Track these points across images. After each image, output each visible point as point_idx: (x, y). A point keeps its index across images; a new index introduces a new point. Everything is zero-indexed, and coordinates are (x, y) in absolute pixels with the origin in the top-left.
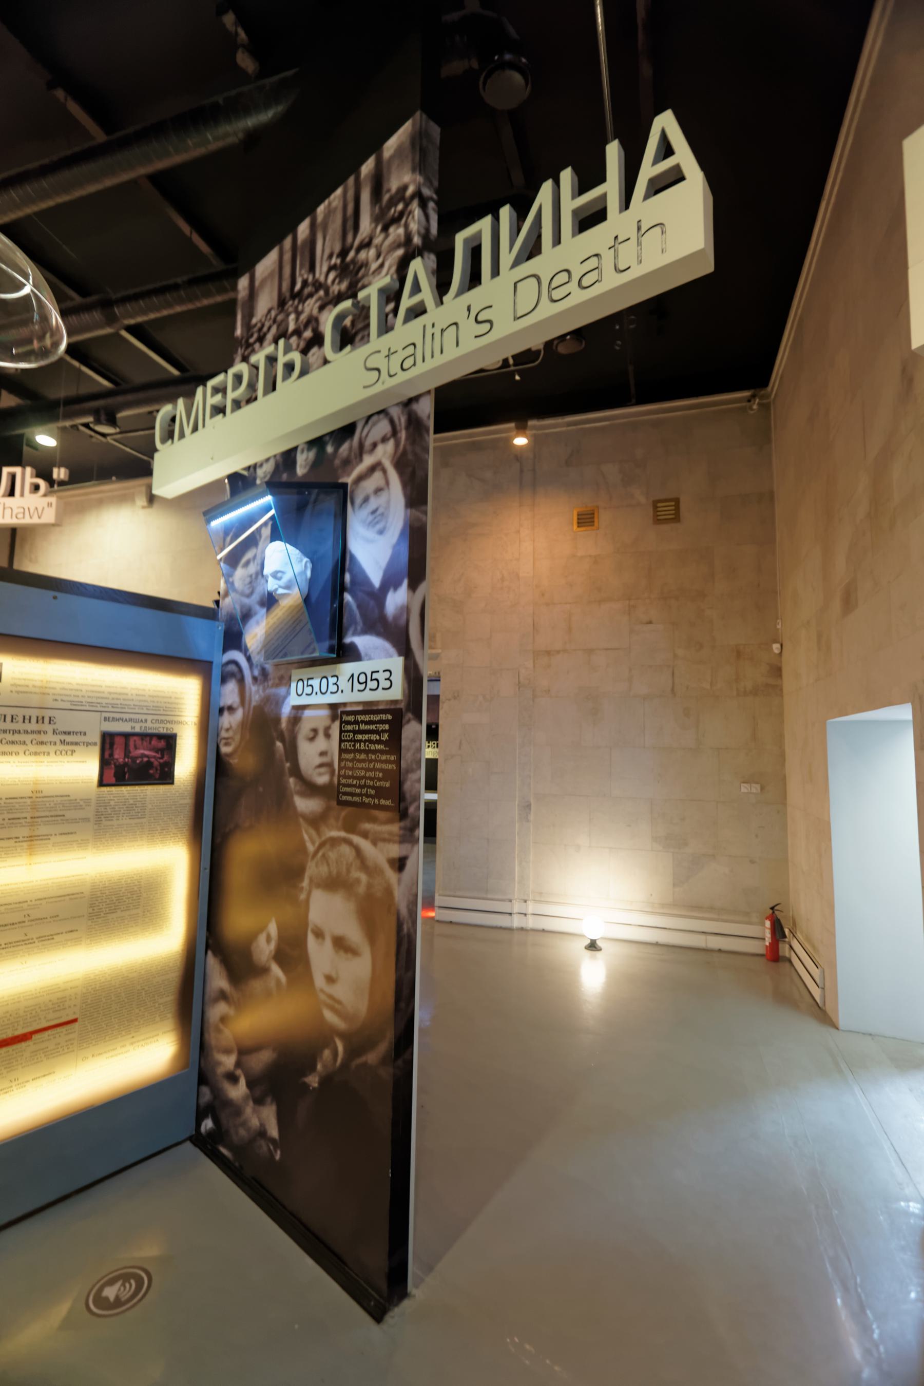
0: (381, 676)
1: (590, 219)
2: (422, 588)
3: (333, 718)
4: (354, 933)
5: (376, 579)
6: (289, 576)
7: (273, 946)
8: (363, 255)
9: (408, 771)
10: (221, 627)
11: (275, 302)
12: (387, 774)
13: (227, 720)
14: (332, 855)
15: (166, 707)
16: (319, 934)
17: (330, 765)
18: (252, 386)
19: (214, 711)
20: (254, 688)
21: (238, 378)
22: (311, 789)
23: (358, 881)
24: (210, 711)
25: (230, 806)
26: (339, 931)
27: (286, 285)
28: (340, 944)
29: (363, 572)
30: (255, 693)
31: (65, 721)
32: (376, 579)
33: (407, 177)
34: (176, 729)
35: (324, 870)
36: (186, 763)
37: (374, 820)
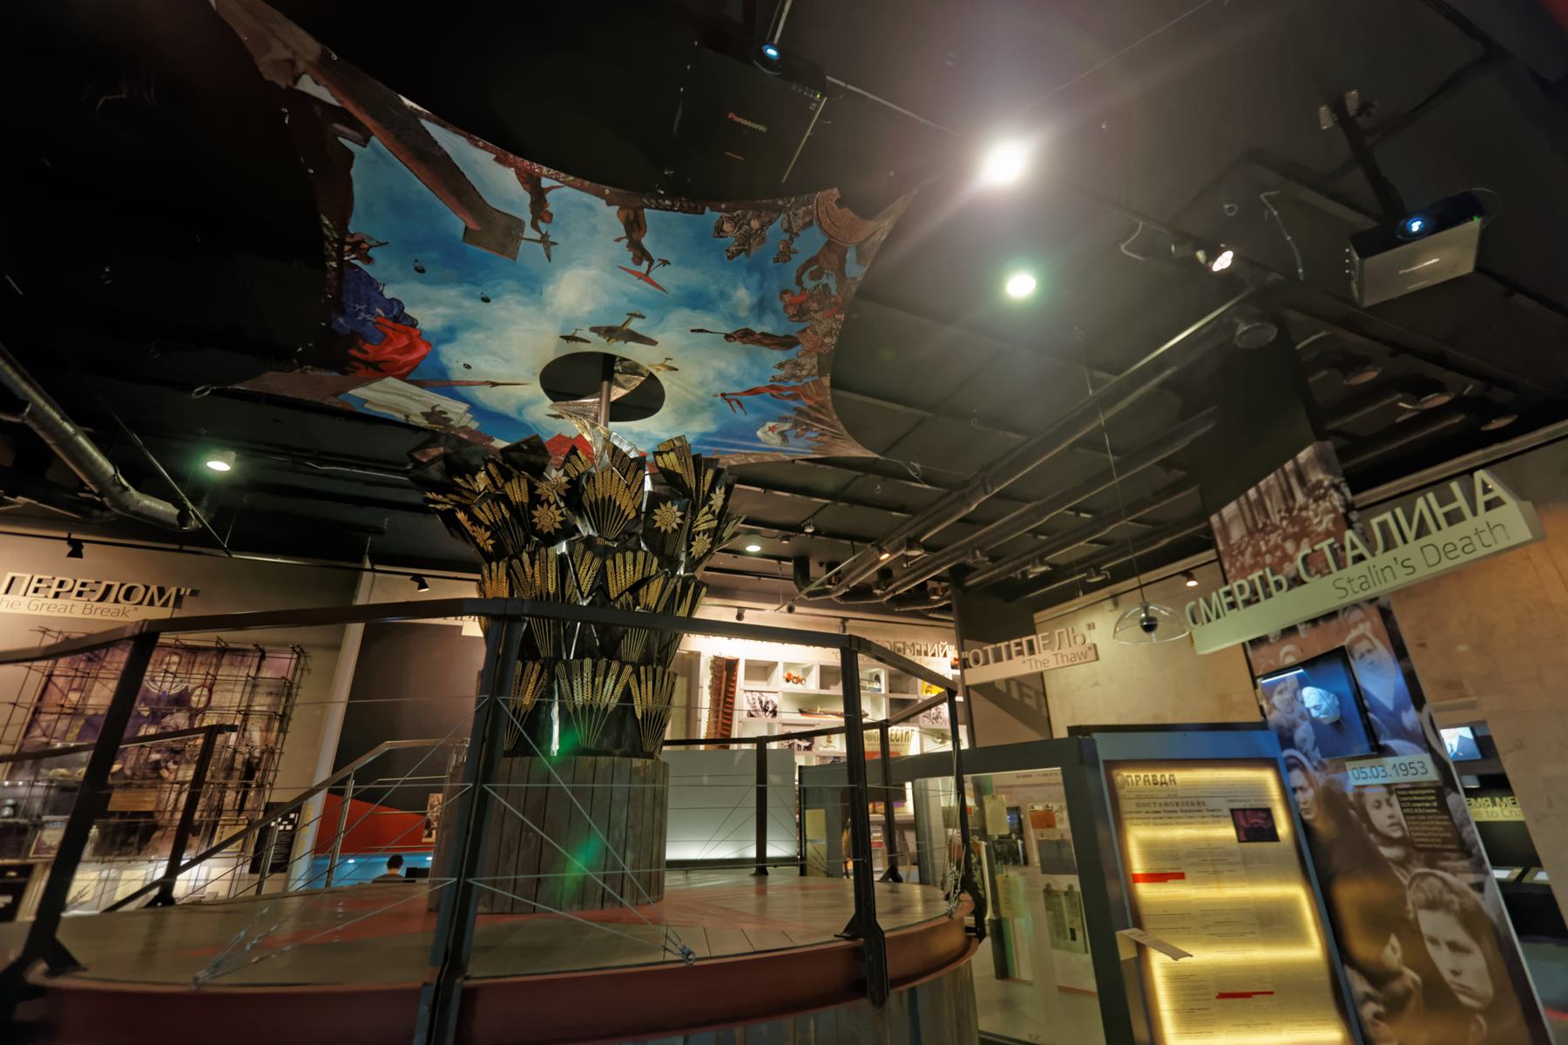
0: (1418, 766)
1: (1454, 518)
2: (1426, 709)
3: (1391, 793)
4: (1461, 936)
5: (1390, 705)
6: (1325, 706)
7: (1399, 954)
8: (1304, 514)
9: (1462, 826)
10: (1274, 735)
11: (1244, 532)
12: (1446, 829)
13: (1300, 796)
14: (1424, 885)
15: (1259, 789)
16: (1434, 942)
17: (1399, 824)
18: (1254, 592)
19: (1290, 792)
20: (1317, 774)
21: (1241, 587)
22: (1390, 841)
23: (1451, 902)
24: (1288, 793)
25: (1319, 864)
26: (1450, 937)
27: (1250, 524)
28: (1454, 946)
29: (1376, 700)
30: (1320, 778)
31: (1212, 803)
32: (1390, 705)
33: (1321, 476)
34: (1269, 805)
35: (1421, 897)
36: (1283, 827)
37: (1447, 859)
